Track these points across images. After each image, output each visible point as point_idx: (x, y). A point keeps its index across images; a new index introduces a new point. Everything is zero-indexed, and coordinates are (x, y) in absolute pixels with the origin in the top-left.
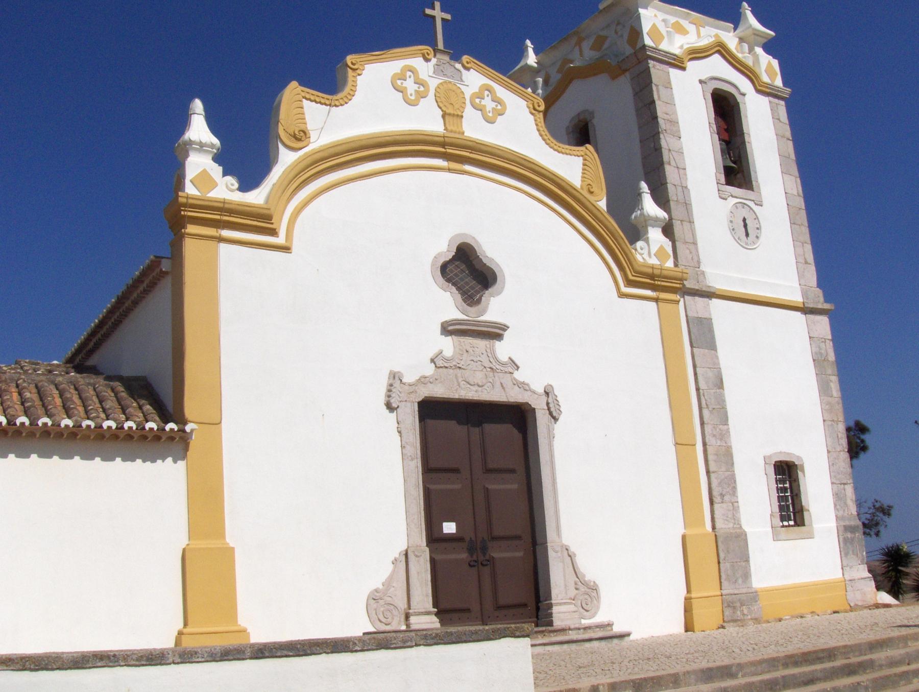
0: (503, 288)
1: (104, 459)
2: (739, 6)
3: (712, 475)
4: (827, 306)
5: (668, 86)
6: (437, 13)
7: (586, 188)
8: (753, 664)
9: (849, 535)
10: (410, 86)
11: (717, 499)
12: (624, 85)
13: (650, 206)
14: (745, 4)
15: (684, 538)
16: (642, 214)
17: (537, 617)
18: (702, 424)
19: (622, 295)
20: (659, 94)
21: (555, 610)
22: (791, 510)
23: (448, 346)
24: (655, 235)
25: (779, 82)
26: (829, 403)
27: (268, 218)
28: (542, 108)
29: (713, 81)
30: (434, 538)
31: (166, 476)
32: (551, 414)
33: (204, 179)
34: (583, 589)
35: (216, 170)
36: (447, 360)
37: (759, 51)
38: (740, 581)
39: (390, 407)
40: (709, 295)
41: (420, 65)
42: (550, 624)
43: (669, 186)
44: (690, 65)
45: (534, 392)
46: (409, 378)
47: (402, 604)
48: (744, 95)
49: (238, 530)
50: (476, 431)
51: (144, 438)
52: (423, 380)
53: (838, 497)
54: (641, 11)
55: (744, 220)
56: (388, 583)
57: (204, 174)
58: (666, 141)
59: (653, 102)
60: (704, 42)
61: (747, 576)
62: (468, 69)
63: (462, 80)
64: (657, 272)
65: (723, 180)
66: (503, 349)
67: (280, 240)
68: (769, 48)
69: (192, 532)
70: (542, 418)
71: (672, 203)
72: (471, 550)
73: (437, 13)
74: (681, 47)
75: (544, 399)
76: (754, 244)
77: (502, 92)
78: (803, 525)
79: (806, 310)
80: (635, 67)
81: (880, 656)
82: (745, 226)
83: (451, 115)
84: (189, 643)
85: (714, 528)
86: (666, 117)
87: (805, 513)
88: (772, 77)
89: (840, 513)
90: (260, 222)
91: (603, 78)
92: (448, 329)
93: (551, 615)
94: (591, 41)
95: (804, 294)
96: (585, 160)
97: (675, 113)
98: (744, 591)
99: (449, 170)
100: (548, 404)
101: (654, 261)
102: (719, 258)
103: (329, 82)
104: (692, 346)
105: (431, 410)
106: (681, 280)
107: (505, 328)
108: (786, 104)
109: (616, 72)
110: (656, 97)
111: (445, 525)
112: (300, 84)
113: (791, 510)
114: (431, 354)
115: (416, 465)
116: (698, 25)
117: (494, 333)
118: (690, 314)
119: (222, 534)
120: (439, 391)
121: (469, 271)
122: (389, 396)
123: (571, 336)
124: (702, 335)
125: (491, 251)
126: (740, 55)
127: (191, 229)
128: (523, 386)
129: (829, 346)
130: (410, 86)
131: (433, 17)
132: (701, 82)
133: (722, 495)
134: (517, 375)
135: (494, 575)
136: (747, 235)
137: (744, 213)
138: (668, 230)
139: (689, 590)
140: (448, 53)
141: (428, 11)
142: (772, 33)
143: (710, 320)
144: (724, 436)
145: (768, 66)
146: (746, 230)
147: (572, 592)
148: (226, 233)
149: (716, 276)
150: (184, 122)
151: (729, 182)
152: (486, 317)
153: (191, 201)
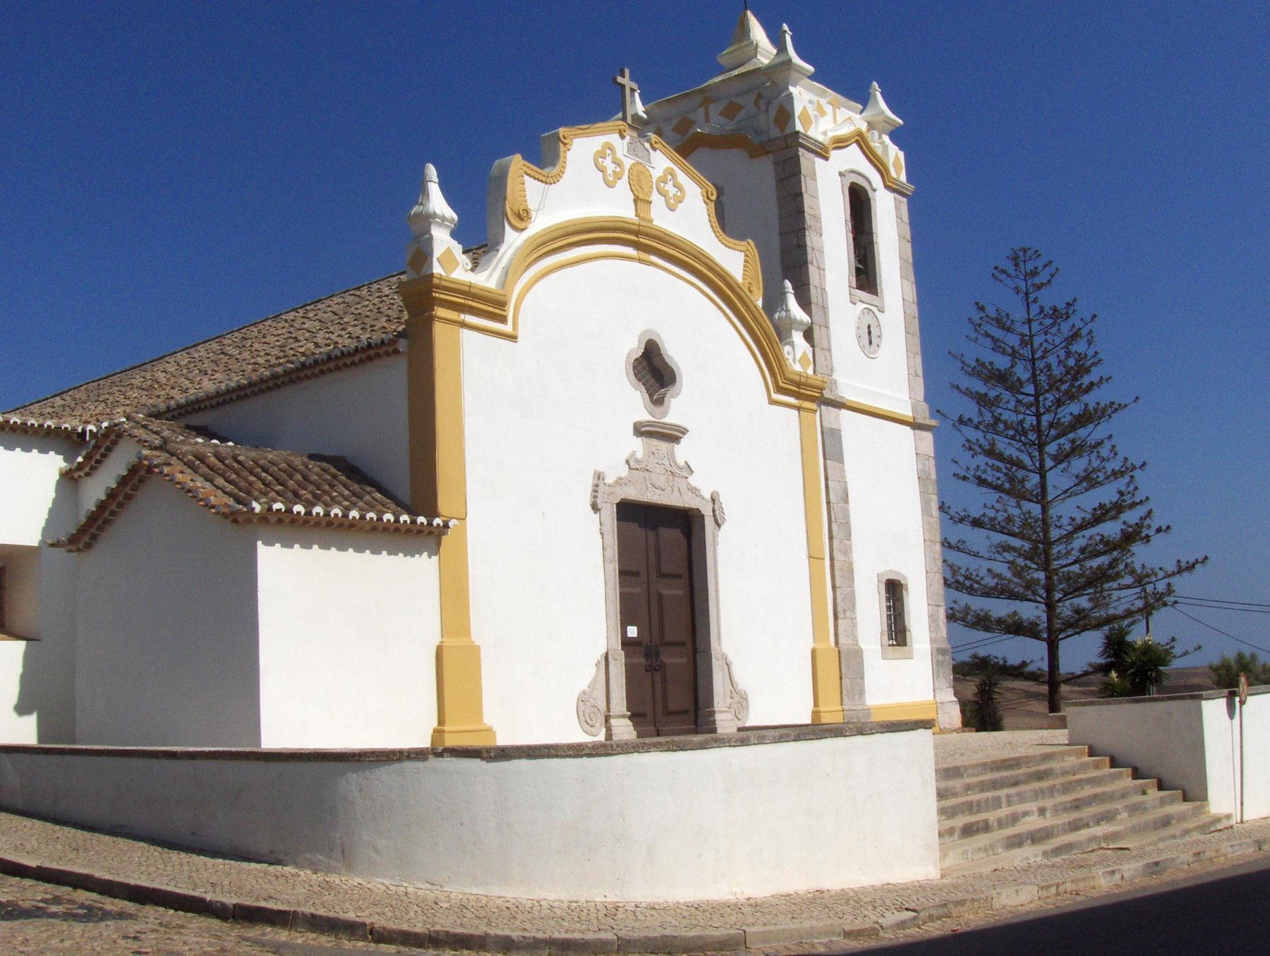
1: (373, 553)
2: (869, 86)
3: (838, 591)
4: (933, 423)
8: (974, 766)
9: (941, 658)
10: (608, 163)
11: (840, 615)
12: (765, 169)
14: (875, 84)
15: (814, 652)
16: (788, 316)
17: (696, 724)
18: (831, 538)
21: (718, 717)
22: (897, 632)
23: (638, 446)
24: (798, 337)
25: (903, 178)
26: (929, 523)
27: (502, 304)
28: (714, 198)
30: (627, 643)
31: (416, 572)
34: (736, 698)
35: (457, 248)
36: (638, 461)
37: (886, 138)
39: (595, 508)
40: (839, 405)
42: (714, 731)
43: (812, 287)
44: (834, 154)
46: (610, 480)
47: (603, 706)
49: (480, 631)
50: (651, 534)
51: (330, 524)
52: (620, 482)
54: (792, 89)
55: (869, 327)
56: (592, 686)
57: (449, 251)
58: (811, 239)
59: (801, 194)
60: (845, 130)
61: (862, 693)
62: (654, 149)
63: (649, 161)
64: (803, 380)
65: (854, 284)
66: (683, 452)
67: (507, 328)
68: (897, 136)
69: (443, 632)
70: (709, 522)
71: (813, 306)
72: (647, 655)
74: (825, 133)
75: (711, 505)
76: (874, 349)
77: (682, 178)
79: (915, 426)
80: (783, 153)
81: (1054, 765)
82: (870, 333)
84: (451, 741)
85: (837, 643)
86: (811, 212)
88: (898, 174)
90: (491, 307)
91: (738, 155)
92: (641, 430)
93: (714, 722)
94: (722, 106)
95: (914, 408)
97: (818, 207)
98: (860, 707)
99: (640, 261)
100: (714, 511)
101: (798, 368)
103: (544, 157)
104: (825, 458)
106: (822, 389)
107: (684, 431)
108: (909, 204)
109: (757, 150)
113: (897, 632)
114: (625, 456)
115: (614, 567)
116: (835, 106)
117: (672, 436)
118: (825, 424)
119: (467, 632)
120: (633, 494)
121: (654, 370)
122: (595, 497)
124: (832, 446)
125: (673, 352)
127: (440, 312)
128: (695, 491)
129: (932, 462)
130: (608, 163)
131: (623, 87)
132: (841, 174)
133: (845, 611)
134: (692, 480)
135: (664, 680)
136: (870, 343)
137: (868, 319)
138: (809, 335)
139: (816, 704)
140: (637, 129)
141: (619, 79)
142: (901, 122)
144: (847, 551)
145: (894, 155)
146: (870, 337)
147: (729, 701)
149: (847, 388)
150: (420, 189)
151: (860, 287)
152: (668, 419)
153: (444, 283)
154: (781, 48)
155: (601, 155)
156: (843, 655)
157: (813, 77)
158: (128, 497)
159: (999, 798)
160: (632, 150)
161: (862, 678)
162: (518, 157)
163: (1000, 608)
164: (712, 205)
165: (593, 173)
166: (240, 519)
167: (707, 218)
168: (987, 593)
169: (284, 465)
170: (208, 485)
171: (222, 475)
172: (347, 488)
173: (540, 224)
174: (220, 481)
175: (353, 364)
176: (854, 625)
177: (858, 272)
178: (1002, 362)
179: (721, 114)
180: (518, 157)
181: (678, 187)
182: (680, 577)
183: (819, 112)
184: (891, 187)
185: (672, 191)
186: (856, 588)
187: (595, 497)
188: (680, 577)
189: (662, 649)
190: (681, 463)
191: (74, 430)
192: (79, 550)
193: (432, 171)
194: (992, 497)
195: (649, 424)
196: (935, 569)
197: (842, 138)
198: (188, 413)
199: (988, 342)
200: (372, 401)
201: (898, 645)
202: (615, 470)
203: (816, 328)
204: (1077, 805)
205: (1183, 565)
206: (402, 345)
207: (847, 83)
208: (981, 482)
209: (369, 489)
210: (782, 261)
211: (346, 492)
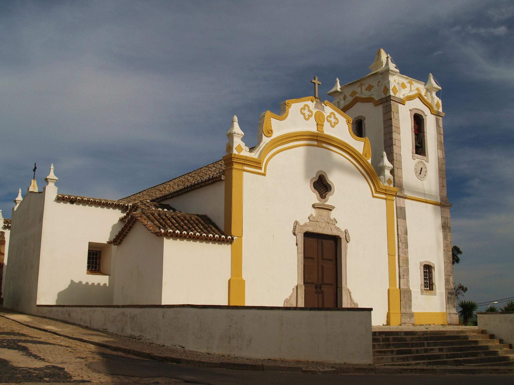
3: (401, 268)
5: (398, 112)
6: (316, 81)
9: (450, 296)
10: (307, 113)
11: (402, 277)
12: (380, 109)
13: (386, 162)
14: (431, 74)
15: (389, 290)
18: (399, 248)
19: (373, 197)
20: (394, 116)
22: (429, 284)
23: (314, 212)
25: (441, 110)
33: (239, 148)
35: (243, 144)
36: (314, 218)
39: (294, 234)
40: (405, 198)
43: (394, 154)
44: (407, 103)
52: (305, 225)
56: (291, 297)
58: (395, 136)
59: (391, 119)
61: (410, 307)
66: (333, 215)
67: (262, 171)
70: (343, 241)
71: (395, 161)
74: (404, 95)
80: (386, 103)
82: (421, 170)
83: (320, 125)
85: (400, 288)
89: (447, 287)
90: (257, 164)
97: (399, 124)
99: (318, 146)
103: (280, 109)
105: (308, 235)
107: (334, 207)
108: (443, 120)
113: (429, 284)
117: (329, 209)
120: (310, 229)
123: (356, 211)
124: (401, 213)
126: (426, 98)
130: (307, 113)
131: (315, 83)
132: (410, 110)
133: (404, 276)
134: (337, 225)
138: (392, 172)
141: (313, 81)
142: (440, 88)
144: (406, 253)
146: (421, 172)
148: (246, 168)
151: (417, 153)
155: (304, 108)
156: (402, 292)
158: (131, 227)
159: (423, 343)
160: (316, 107)
161: (411, 301)
164: (350, 125)
169: (182, 218)
171: (158, 221)
173: (276, 135)
174: (156, 222)
175: (209, 184)
176: (408, 281)
179: (366, 90)
180: (268, 111)
181: (335, 118)
182: (332, 260)
189: (322, 286)
191: (124, 205)
192: (117, 245)
196: (449, 262)
201: (430, 290)
202: (303, 220)
204: (454, 349)
205: (459, 256)
206: (223, 178)
209: (211, 226)
210: (385, 144)
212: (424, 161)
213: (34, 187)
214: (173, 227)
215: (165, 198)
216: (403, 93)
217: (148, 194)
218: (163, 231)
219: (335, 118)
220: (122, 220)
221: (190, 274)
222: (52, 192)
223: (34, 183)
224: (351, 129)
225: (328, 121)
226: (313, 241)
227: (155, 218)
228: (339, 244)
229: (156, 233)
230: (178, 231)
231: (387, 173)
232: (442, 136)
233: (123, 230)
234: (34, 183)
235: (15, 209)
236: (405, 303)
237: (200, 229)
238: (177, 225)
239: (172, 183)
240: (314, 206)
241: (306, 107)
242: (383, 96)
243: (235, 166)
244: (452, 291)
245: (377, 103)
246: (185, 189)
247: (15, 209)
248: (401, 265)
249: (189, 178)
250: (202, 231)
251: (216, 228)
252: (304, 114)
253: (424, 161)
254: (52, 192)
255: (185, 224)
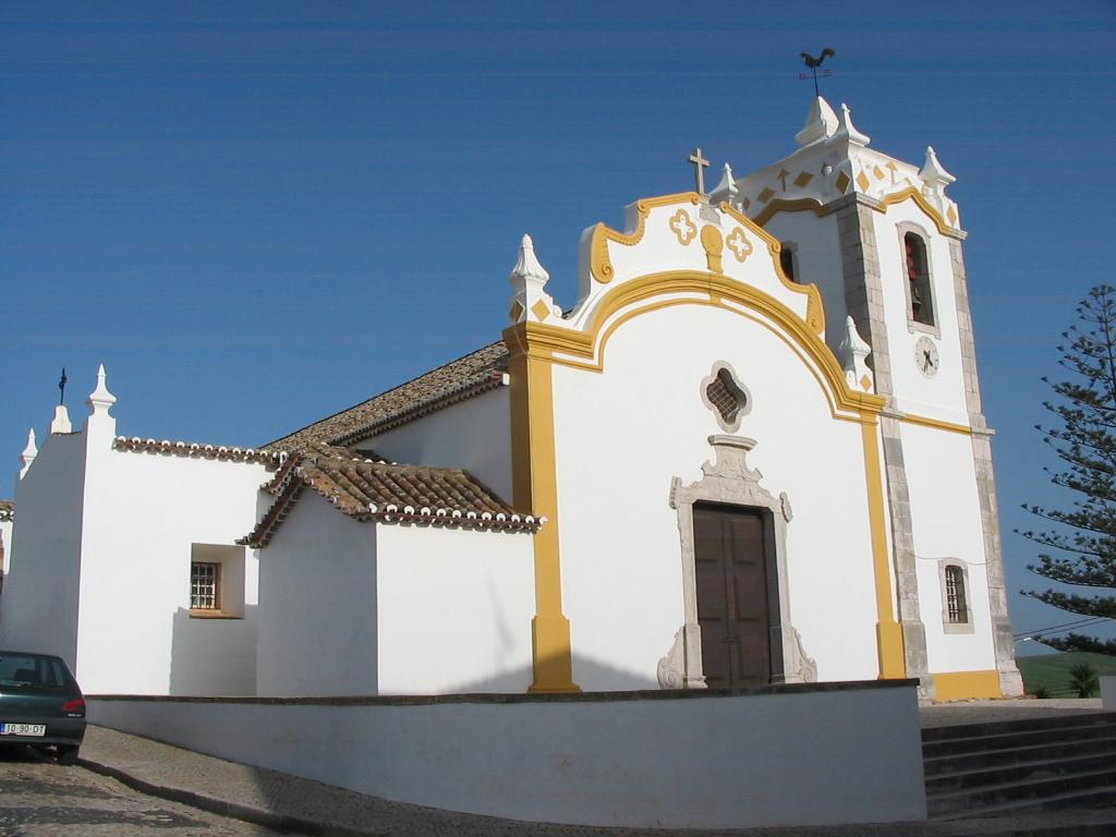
0: (750, 409)
5: (871, 230)
6: (699, 159)
7: (810, 321)
9: (1002, 633)
10: (685, 229)
11: (903, 596)
15: (878, 626)
19: (835, 417)
22: (958, 611)
23: (712, 455)
25: (957, 225)
29: (910, 225)
32: (785, 516)
33: (541, 309)
35: (548, 300)
36: (713, 469)
38: (919, 666)
41: (692, 208)
43: (865, 262)
44: (890, 208)
45: (772, 498)
46: (686, 483)
48: (930, 237)
52: (695, 485)
53: (994, 600)
56: (672, 653)
58: (869, 280)
60: (901, 187)
61: (924, 662)
62: (724, 212)
63: (720, 223)
65: (912, 317)
66: (752, 460)
67: (595, 362)
68: (950, 191)
70: (778, 519)
73: (699, 159)
74: (882, 192)
76: (932, 371)
78: (966, 622)
80: (845, 212)
83: (713, 255)
85: (900, 620)
87: (968, 612)
88: (953, 223)
89: (994, 614)
90: (581, 345)
96: (809, 297)
97: (877, 255)
99: (712, 304)
101: (860, 389)
102: (908, 387)
103: (624, 223)
105: (700, 506)
107: (754, 443)
110: (862, 240)
111: (907, 558)
112: (606, 226)
113: (958, 611)
115: (691, 555)
121: (726, 394)
125: (742, 378)
128: (765, 492)
130: (685, 229)
132: (896, 225)
134: (761, 483)
138: (869, 361)
141: (692, 158)
142: (954, 179)
143: (899, 441)
144: (907, 541)
145: (948, 207)
148: (556, 355)
154: (842, 123)
155: (676, 219)
157: (868, 146)
158: (292, 504)
160: (703, 215)
162: (601, 225)
163: (1088, 593)
165: (666, 235)
166: (364, 518)
167: (773, 267)
168: (1079, 580)
170: (345, 492)
172: (462, 494)
173: (620, 277)
176: (916, 605)
177: (915, 307)
178: (1083, 382)
180: (601, 225)
181: (745, 241)
182: (752, 564)
183: (875, 173)
184: (943, 231)
185: (740, 246)
186: (917, 572)
187: (673, 498)
188: (752, 564)
190: (752, 470)
192: (259, 547)
193: (527, 241)
194: (1083, 497)
195: (720, 437)
197: (898, 195)
198: (359, 440)
199: (1073, 365)
200: (483, 424)
201: (960, 621)
202: (691, 475)
203: (875, 354)
207: (899, 144)
208: (1075, 486)
211: (460, 498)
212: (932, 337)
213: (62, 423)
214: (395, 499)
215: (362, 436)
216: (878, 189)
217: (315, 433)
218: (374, 508)
219: (745, 241)
220: (265, 490)
221: (442, 610)
222: (102, 428)
223: (62, 412)
224: (779, 264)
225: (730, 247)
226: (708, 516)
227: (350, 480)
228: (767, 522)
229: (358, 514)
230: (409, 509)
231: (859, 361)
232: (964, 282)
233: (273, 511)
234: (62, 412)
235: (22, 477)
236: (914, 654)
237: (458, 502)
238: (403, 494)
239: (368, 408)
240: (711, 441)
241: (682, 216)
242: (837, 195)
243: (533, 350)
244: (1004, 623)
245: (823, 212)
246: (401, 416)
247: (22, 477)
248: (900, 570)
249: (409, 392)
250: (464, 506)
251: (505, 496)
252: (678, 232)
253: (932, 337)
254: (102, 428)
255: (422, 492)
